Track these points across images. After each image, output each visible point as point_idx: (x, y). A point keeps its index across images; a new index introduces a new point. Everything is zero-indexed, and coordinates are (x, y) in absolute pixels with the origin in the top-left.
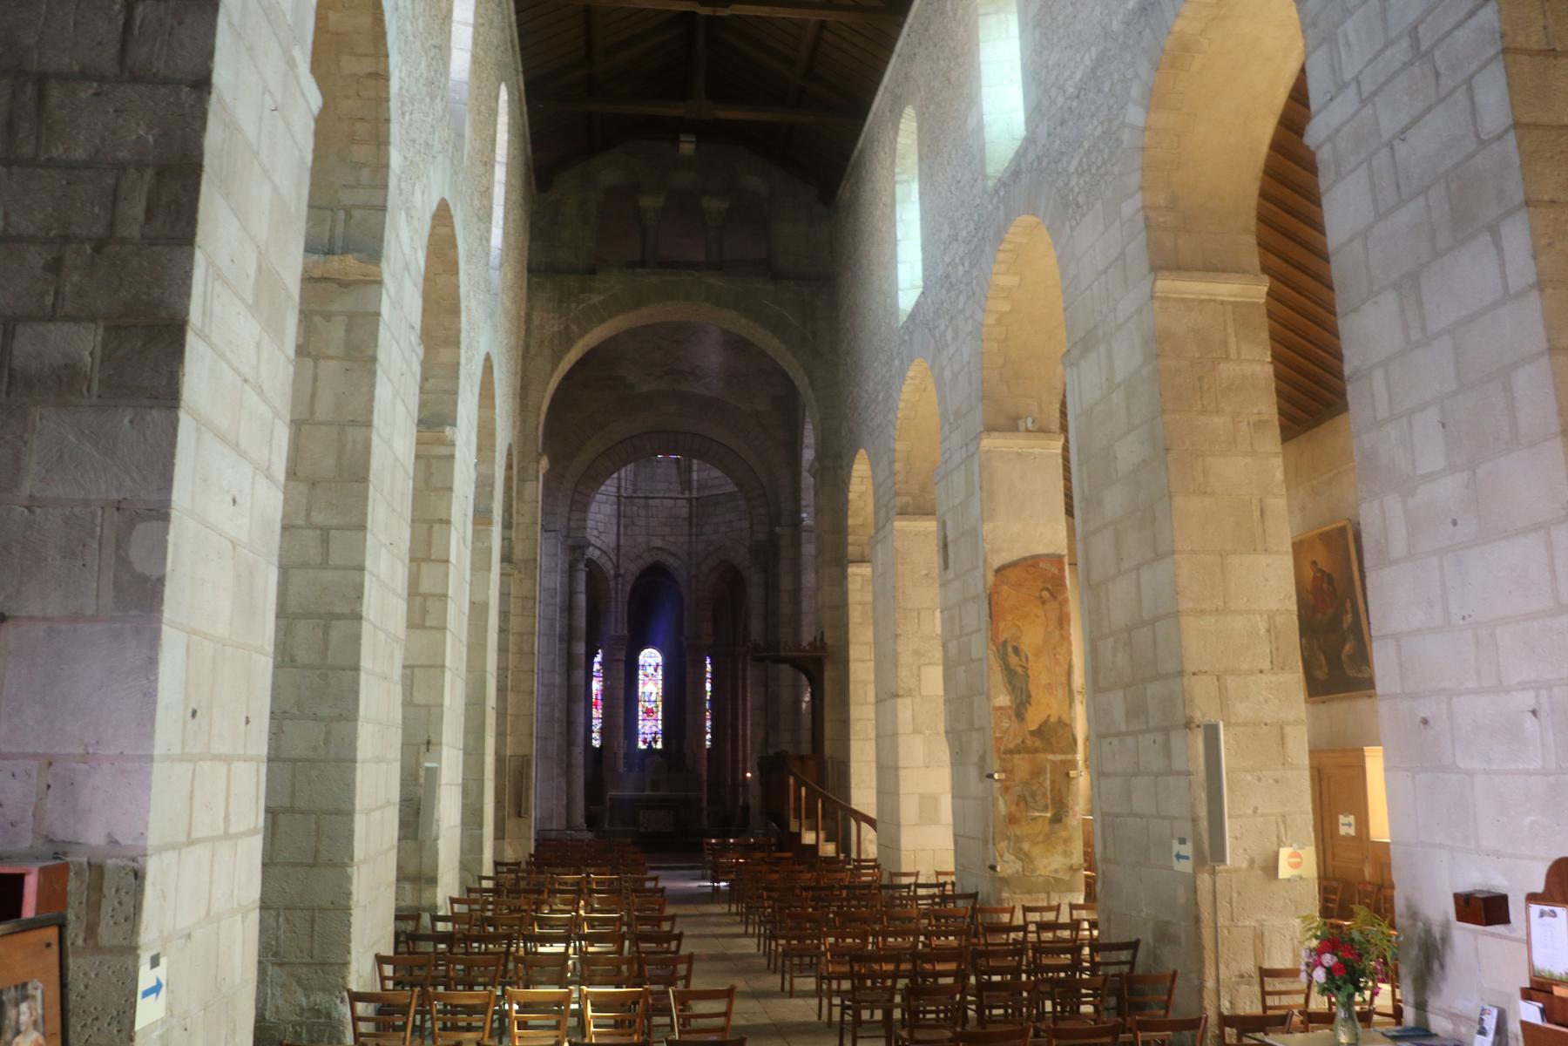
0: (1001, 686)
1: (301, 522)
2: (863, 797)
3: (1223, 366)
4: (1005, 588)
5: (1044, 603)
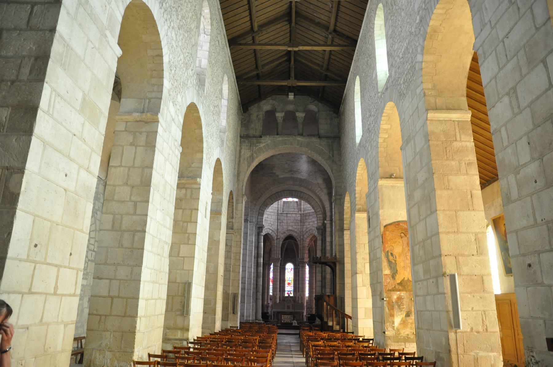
0: (386, 267)
1: (128, 200)
2: (348, 310)
3: (455, 143)
4: (387, 233)
5: (402, 238)
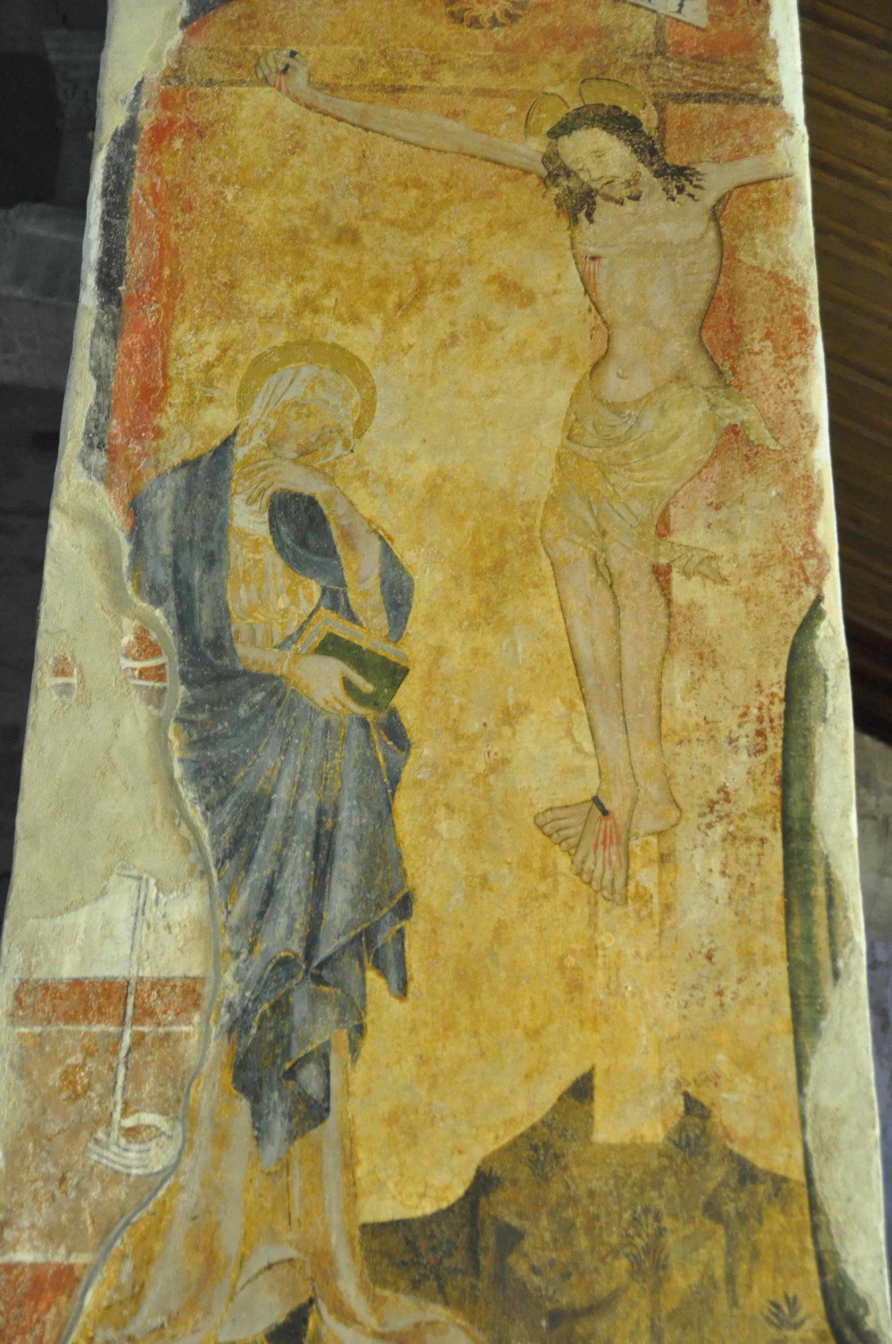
5: (580, 204)
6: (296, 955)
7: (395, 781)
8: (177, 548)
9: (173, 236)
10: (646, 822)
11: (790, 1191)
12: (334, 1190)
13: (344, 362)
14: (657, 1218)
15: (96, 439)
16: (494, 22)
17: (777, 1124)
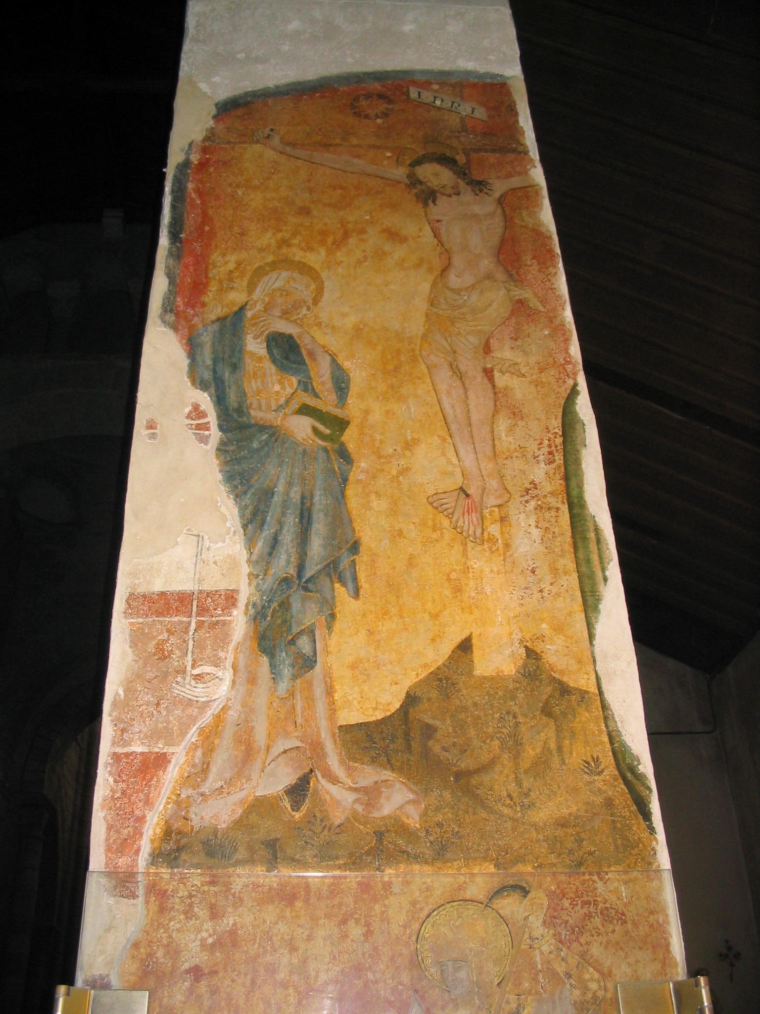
6: (292, 576)
7: (345, 480)
8: (215, 361)
9: (210, 212)
10: (492, 501)
11: (590, 698)
12: (321, 707)
13: (305, 269)
14: (515, 717)
15: (168, 307)
16: (377, 117)
17: (580, 662)
